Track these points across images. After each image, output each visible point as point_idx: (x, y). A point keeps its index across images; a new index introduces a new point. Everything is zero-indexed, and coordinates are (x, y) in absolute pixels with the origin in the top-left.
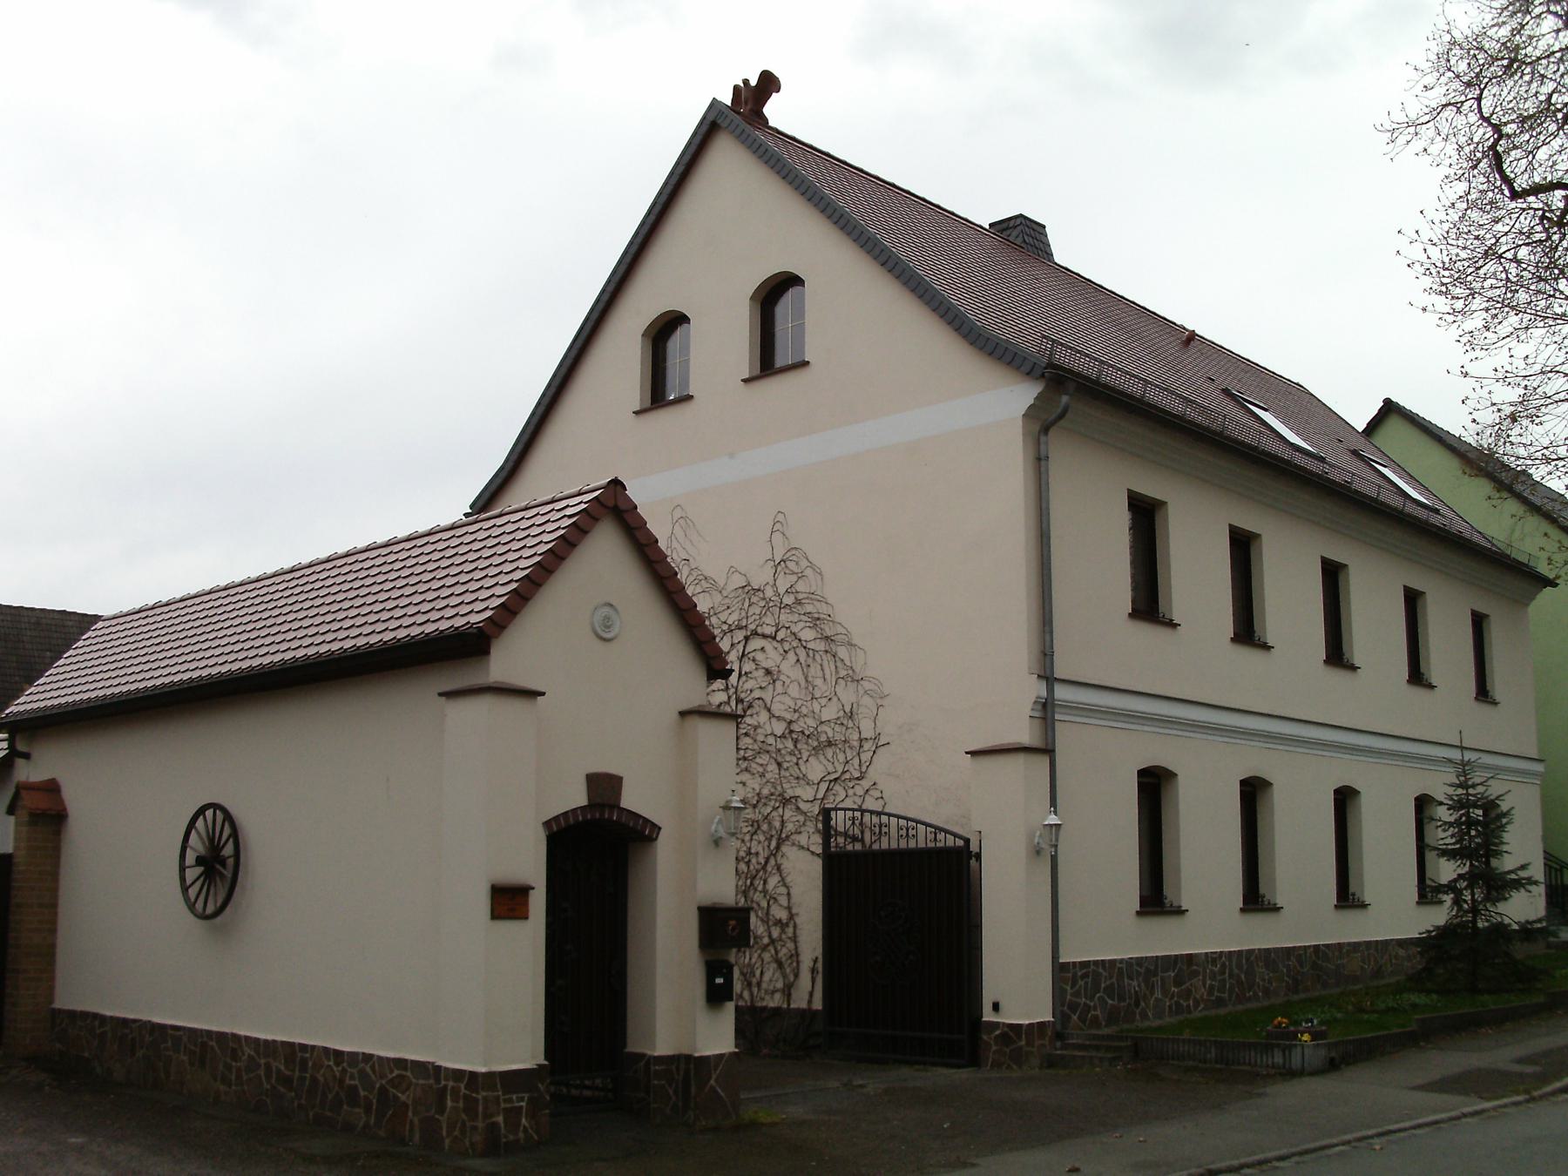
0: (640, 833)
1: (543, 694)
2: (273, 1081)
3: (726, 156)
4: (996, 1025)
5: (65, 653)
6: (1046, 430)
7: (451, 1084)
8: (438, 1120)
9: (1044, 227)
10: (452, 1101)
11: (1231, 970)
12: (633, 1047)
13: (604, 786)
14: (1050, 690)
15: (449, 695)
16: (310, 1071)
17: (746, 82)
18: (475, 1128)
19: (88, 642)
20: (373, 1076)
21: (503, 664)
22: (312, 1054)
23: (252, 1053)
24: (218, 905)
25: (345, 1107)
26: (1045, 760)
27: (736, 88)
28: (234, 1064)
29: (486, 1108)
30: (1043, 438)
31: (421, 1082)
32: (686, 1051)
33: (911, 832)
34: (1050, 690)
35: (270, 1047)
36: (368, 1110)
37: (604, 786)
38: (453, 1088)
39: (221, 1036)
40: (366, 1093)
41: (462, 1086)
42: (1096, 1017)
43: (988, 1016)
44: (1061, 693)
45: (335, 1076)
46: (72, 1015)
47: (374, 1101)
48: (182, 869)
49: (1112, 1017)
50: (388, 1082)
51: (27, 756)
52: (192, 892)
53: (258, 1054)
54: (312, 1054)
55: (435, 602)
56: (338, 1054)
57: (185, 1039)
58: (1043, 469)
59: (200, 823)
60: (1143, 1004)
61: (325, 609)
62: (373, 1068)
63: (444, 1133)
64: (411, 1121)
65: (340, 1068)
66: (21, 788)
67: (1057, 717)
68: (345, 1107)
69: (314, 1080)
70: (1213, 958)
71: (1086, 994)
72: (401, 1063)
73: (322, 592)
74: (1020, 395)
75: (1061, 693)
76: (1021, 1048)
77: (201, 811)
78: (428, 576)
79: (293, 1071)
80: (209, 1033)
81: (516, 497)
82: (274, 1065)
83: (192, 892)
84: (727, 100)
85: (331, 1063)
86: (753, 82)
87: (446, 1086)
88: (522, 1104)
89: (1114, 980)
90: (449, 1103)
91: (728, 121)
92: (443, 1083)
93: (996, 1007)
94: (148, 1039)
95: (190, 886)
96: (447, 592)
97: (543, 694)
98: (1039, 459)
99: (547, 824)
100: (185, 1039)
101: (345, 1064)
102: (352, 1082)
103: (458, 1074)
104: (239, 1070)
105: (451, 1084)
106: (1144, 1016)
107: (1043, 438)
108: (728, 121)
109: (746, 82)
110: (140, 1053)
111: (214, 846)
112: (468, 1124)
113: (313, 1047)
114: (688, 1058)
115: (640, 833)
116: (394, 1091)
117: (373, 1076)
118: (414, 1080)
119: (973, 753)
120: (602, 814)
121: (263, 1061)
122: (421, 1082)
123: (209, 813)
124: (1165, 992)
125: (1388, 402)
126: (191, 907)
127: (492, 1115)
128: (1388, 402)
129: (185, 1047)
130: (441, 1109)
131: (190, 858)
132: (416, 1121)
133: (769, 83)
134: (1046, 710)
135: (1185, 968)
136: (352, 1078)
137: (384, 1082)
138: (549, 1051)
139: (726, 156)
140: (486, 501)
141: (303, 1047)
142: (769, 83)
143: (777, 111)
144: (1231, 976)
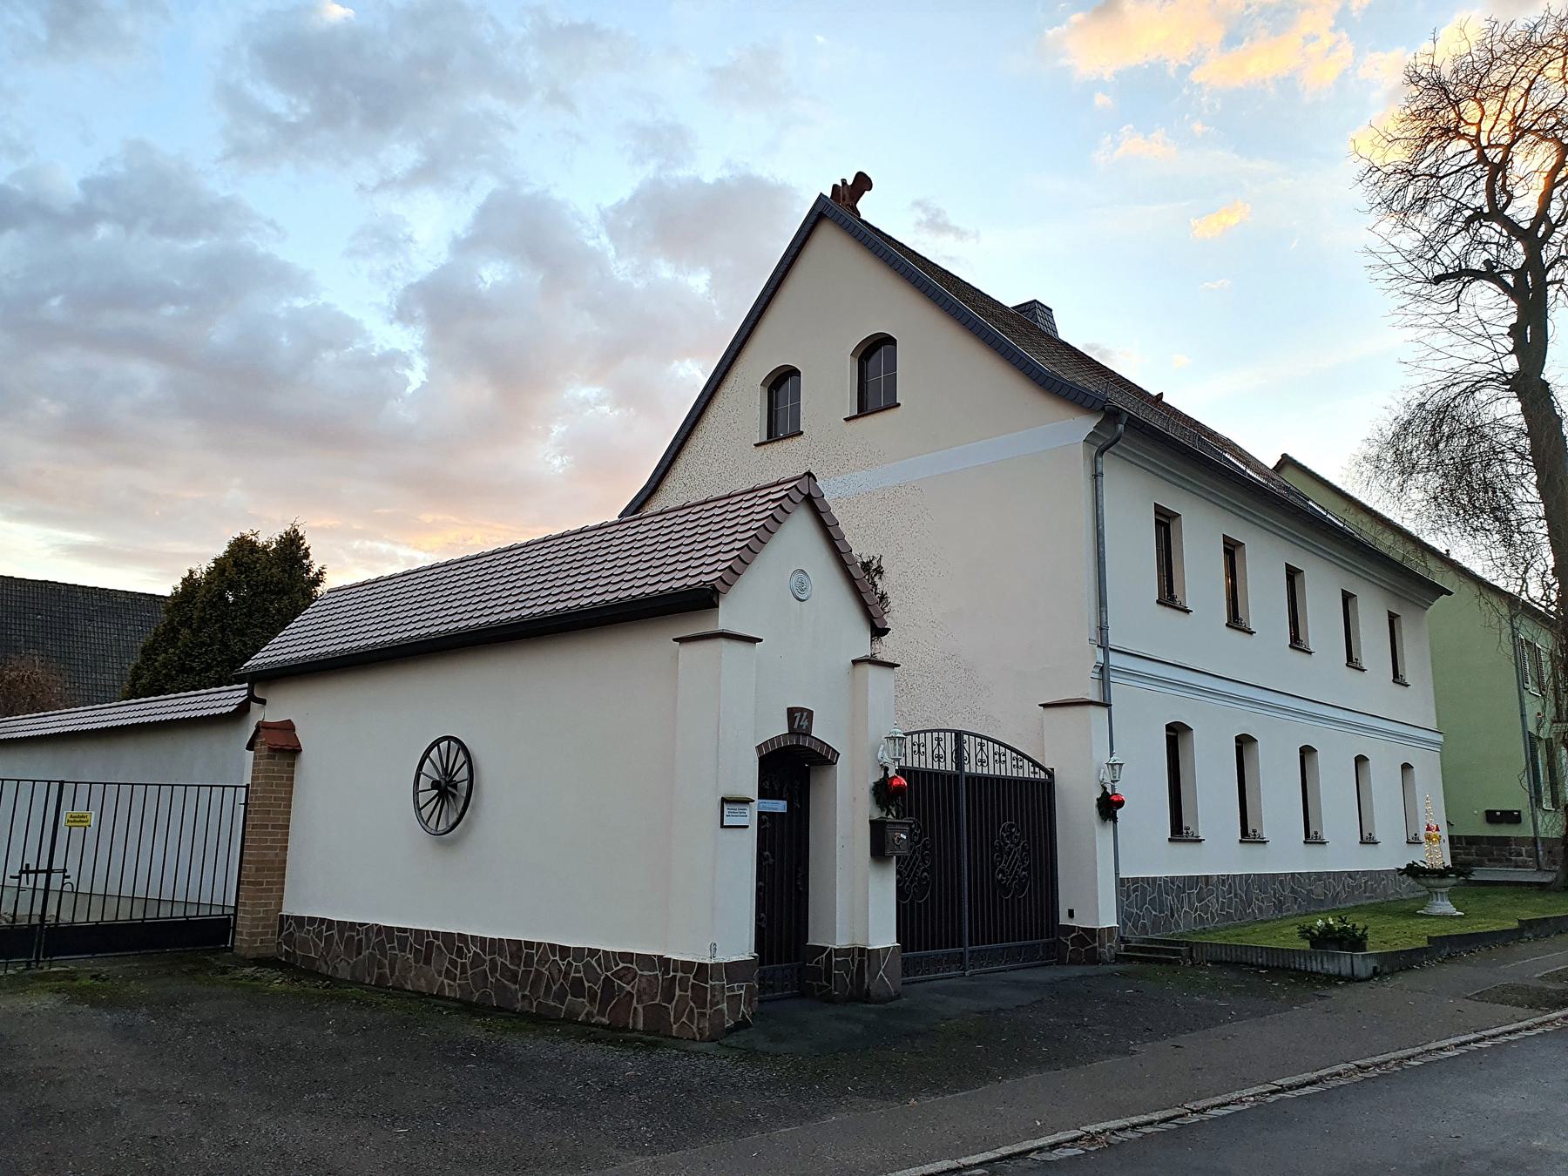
0: (824, 758)
1: (761, 640)
2: (498, 975)
3: (827, 236)
4: (1073, 929)
5: (304, 610)
6: (1101, 452)
7: (679, 974)
8: (667, 1008)
9: (1051, 310)
10: (681, 990)
11: (1236, 891)
12: (813, 941)
13: (799, 718)
14: (1106, 657)
15: (681, 640)
16: (535, 966)
17: (844, 182)
18: (703, 1015)
19: (316, 610)
20: (598, 969)
21: (728, 616)
22: (537, 952)
23: (478, 951)
24: (450, 824)
25: (569, 997)
26: (1106, 711)
27: (835, 186)
28: (459, 960)
29: (713, 996)
30: (1099, 459)
31: (646, 973)
32: (860, 943)
33: (1020, 764)
34: (1106, 657)
35: (495, 945)
36: (592, 1000)
37: (799, 718)
38: (682, 977)
39: (448, 936)
40: (590, 984)
41: (691, 976)
42: (1144, 924)
43: (1064, 920)
44: (1115, 660)
45: (560, 970)
46: (300, 921)
47: (599, 991)
48: (416, 793)
49: (1156, 925)
50: (612, 974)
51: (263, 702)
52: (425, 813)
53: (483, 950)
54: (537, 952)
55: (533, 608)
56: (564, 950)
57: (411, 940)
58: (1099, 483)
59: (434, 753)
60: (1176, 916)
61: (399, 622)
62: (598, 961)
63: (672, 1020)
64: (635, 1008)
65: (565, 963)
66: (261, 727)
67: (1112, 679)
68: (569, 997)
69: (539, 973)
70: (1223, 879)
71: (1137, 904)
72: (626, 957)
73: (415, 606)
74: (1086, 424)
75: (1115, 660)
76: (1095, 948)
77: (436, 743)
78: (517, 591)
79: (519, 966)
80: (435, 934)
81: (655, 506)
82: (499, 960)
83: (425, 813)
84: (829, 194)
85: (557, 958)
86: (850, 182)
87: (675, 977)
88: (741, 992)
89: (1155, 895)
90: (678, 992)
91: (833, 212)
92: (672, 974)
93: (1071, 914)
94: (374, 940)
95: (423, 808)
96: (509, 607)
97: (761, 640)
98: (1096, 476)
99: (759, 748)
100: (411, 940)
101: (570, 959)
102: (577, 975)
103: (687, 966)
104: (463, 965)
105: (679, 974)
106: (1177, 925)
107: (1099, 459)
108: (833, 212)
109: (844, 182)
110: (365, 953)
111: (447, 772)
112: (696, 1011)
113: (539, 944)
114: (862, 951)
115: (824, 758)
116: (619, 982)
117: (598, 969)
118: (639, 972)
119: (1045, 706)
120: (798, 740)
121: (488, 958)
122: (646, 973)
123: (444, 745)
124: (1191, 905)
125: (1284, 456)
126: (425, 823)
127: (718, 1003)
128: (1284, 456)
129: (411, 945)
130: (669, 997)
131: (424, 783)
132: (641, 1010)
133: (863, 183)
134: (1103, 670)
135: (1204, 887)
136: (577, 971)
137: (609, 974)
138: (759, 946)
139: (828, 238)
140: (638, 506)
141: (529, 945)
142: (863, 183)
143: (869, 208)
144: (1236, 895)
